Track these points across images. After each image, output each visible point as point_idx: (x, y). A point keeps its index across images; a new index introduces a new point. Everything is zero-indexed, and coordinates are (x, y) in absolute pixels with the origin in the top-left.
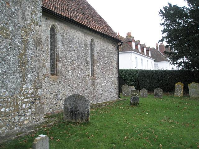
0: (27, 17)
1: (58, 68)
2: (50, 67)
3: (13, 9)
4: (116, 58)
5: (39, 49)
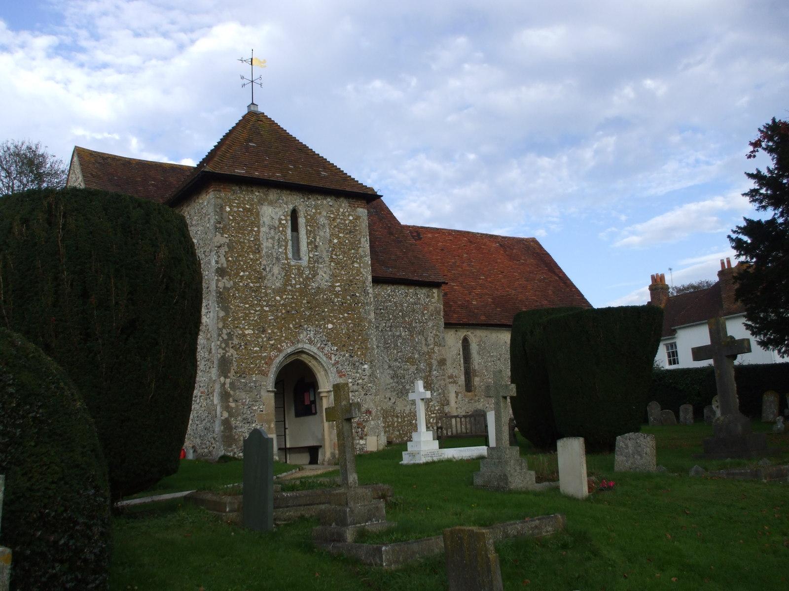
0: (429, 342)
1: (475, 383)
2: (464, 383)
3: (417, 340)
4: (283, 415)
5: (444, 368)
